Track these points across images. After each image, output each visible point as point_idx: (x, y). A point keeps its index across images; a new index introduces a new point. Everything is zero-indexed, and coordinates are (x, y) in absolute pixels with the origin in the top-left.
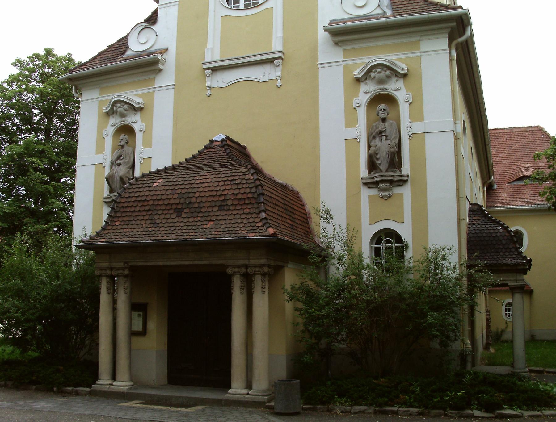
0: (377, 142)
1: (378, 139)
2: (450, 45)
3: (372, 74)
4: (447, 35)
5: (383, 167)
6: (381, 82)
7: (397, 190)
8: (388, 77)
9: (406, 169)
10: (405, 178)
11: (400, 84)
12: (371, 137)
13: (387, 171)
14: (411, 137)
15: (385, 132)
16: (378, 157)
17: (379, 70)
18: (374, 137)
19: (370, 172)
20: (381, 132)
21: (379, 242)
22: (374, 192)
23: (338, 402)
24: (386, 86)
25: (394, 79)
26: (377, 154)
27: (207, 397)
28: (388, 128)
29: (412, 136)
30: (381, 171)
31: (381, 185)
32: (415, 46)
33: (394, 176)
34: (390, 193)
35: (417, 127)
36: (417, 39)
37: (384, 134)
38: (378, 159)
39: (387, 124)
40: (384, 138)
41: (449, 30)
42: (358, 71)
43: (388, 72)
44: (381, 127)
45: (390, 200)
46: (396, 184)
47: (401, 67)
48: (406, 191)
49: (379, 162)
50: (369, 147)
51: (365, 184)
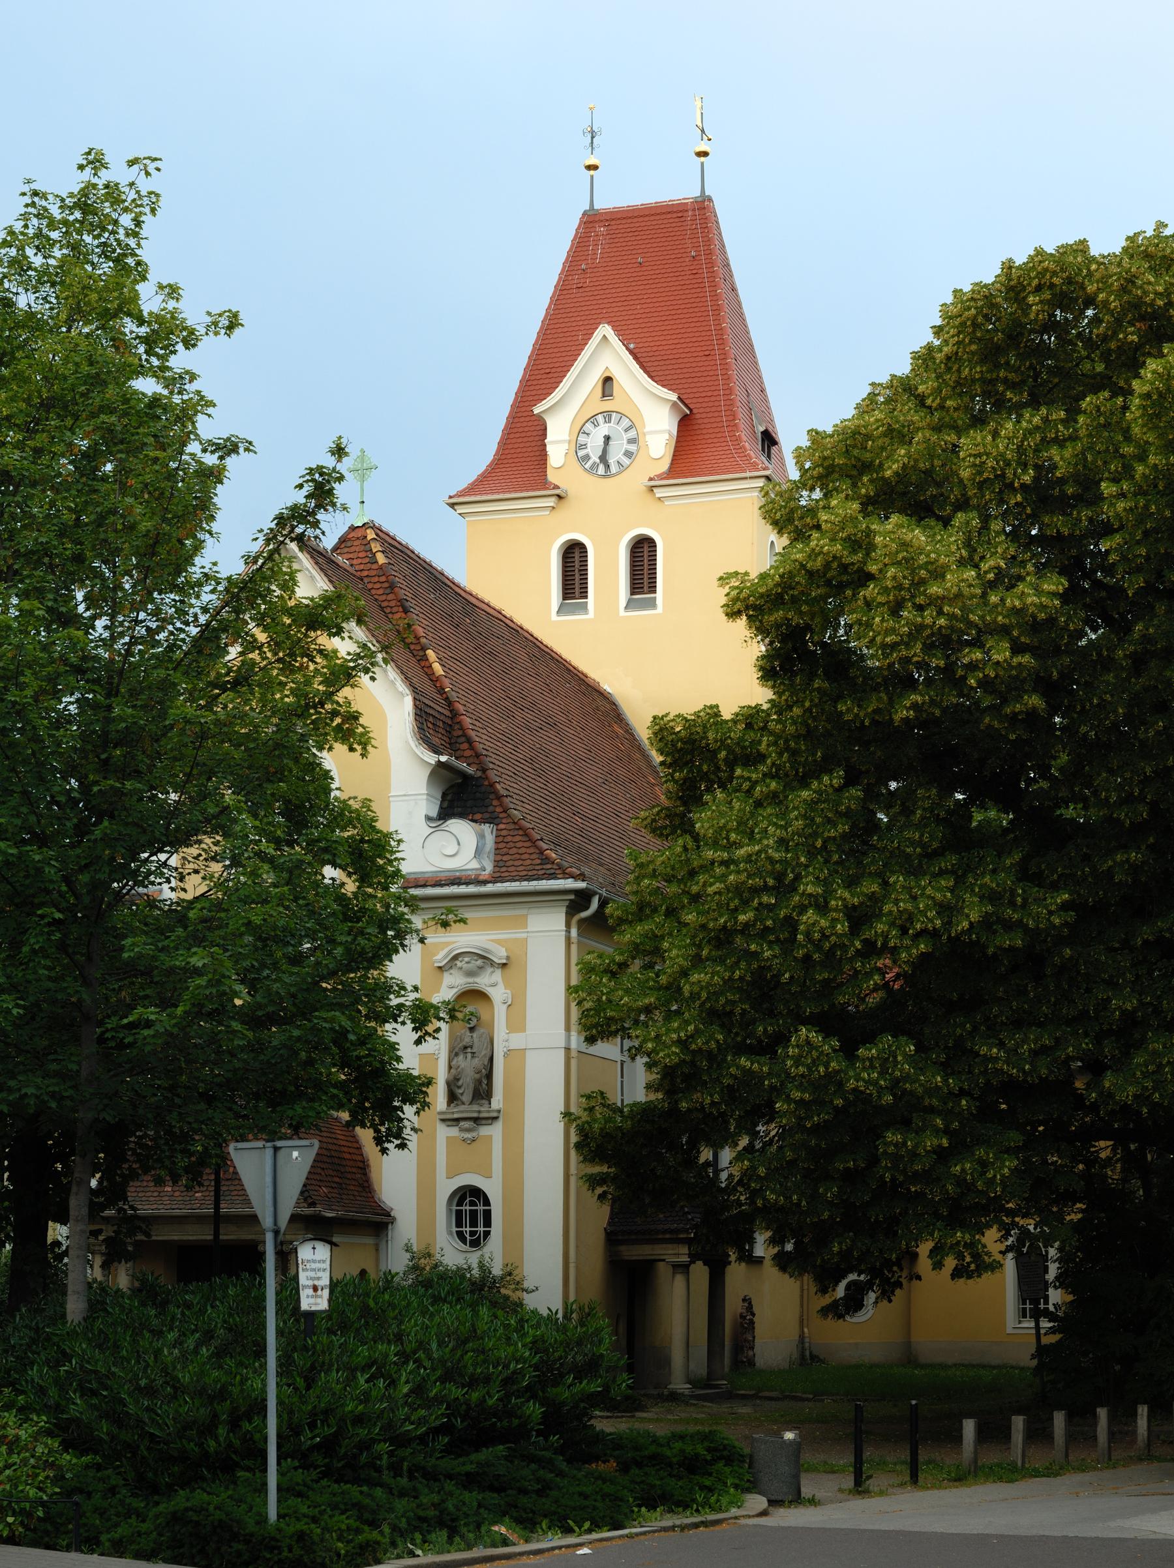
0: (460, 1060)
1: (461, 1057)
2: (568, 925)
3: (459, 964)
4: (564, 909)
5: (466, 1098)
6: (470, 974)
7: (484, 1131)
8: (481, 968)
9: (497, 1101)
10: (495, 1115)
11: (497, 976)
12: (453, 1053)
13: (471, 1103)
14: (506, 1055)
15: (471, 1047)
16: (460, 1083)
17: (466, 959)
18: (457, 1055)
19: (449, 1105)
20: (466, 1048)
21: (460, 1204)
22: (454, 1132)
23: (13, 791)
24: (477, 980)
25: (490, 970)
26: (458, 1080)
27: (513, 884)
28: (476, 1040)
29: (508, 1054)
30: (463, 1103)
31: (462, 1123)
32: (522, 922)
33: (479, 1112)
34: (474, 1134)
35: (517, 1041)
36: (524, 912)
37: (469, 1050)
38: (459, 1087)
39: (475, 1035)
40: (469, 1055)
41: (567, 903)
42: (439, 957)
43: (480, 962)
44: (467, 1040)
45: (474, 1144)
46: (484, 1122)
47: (499, 954)
48: (495, 1132)
49: (461, 1091)
50: (450, 1067)
51: (443, 1120)
